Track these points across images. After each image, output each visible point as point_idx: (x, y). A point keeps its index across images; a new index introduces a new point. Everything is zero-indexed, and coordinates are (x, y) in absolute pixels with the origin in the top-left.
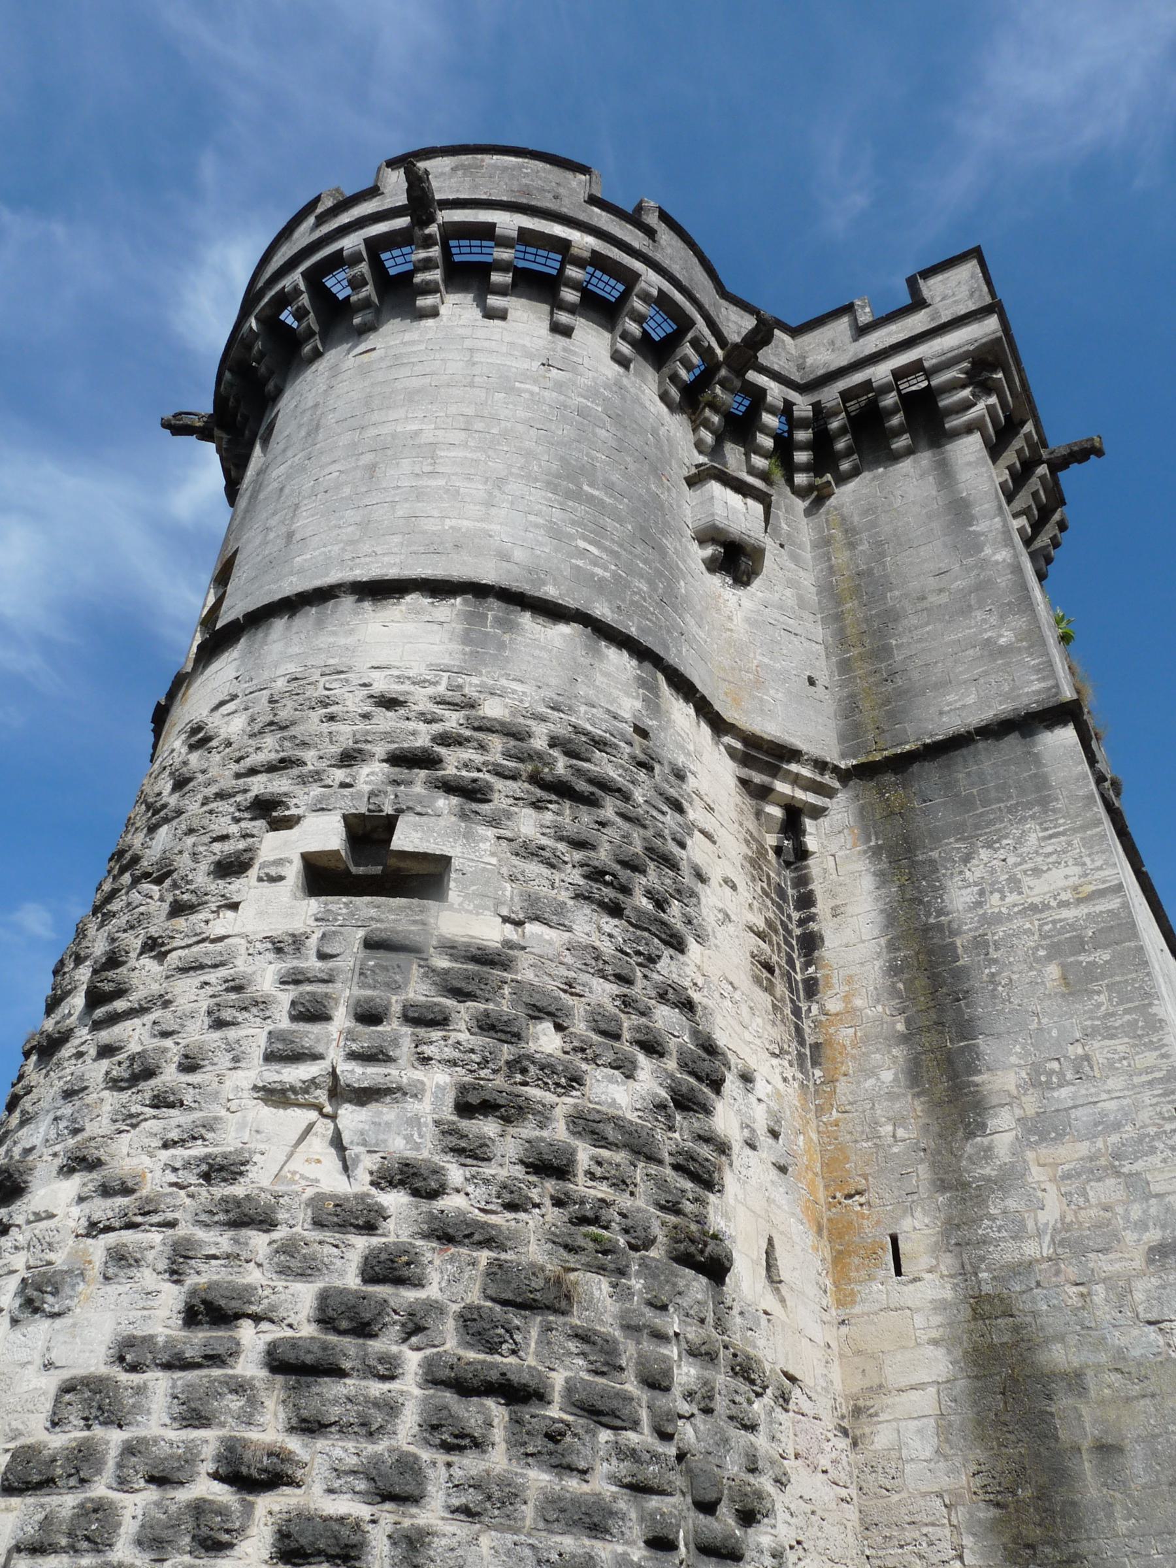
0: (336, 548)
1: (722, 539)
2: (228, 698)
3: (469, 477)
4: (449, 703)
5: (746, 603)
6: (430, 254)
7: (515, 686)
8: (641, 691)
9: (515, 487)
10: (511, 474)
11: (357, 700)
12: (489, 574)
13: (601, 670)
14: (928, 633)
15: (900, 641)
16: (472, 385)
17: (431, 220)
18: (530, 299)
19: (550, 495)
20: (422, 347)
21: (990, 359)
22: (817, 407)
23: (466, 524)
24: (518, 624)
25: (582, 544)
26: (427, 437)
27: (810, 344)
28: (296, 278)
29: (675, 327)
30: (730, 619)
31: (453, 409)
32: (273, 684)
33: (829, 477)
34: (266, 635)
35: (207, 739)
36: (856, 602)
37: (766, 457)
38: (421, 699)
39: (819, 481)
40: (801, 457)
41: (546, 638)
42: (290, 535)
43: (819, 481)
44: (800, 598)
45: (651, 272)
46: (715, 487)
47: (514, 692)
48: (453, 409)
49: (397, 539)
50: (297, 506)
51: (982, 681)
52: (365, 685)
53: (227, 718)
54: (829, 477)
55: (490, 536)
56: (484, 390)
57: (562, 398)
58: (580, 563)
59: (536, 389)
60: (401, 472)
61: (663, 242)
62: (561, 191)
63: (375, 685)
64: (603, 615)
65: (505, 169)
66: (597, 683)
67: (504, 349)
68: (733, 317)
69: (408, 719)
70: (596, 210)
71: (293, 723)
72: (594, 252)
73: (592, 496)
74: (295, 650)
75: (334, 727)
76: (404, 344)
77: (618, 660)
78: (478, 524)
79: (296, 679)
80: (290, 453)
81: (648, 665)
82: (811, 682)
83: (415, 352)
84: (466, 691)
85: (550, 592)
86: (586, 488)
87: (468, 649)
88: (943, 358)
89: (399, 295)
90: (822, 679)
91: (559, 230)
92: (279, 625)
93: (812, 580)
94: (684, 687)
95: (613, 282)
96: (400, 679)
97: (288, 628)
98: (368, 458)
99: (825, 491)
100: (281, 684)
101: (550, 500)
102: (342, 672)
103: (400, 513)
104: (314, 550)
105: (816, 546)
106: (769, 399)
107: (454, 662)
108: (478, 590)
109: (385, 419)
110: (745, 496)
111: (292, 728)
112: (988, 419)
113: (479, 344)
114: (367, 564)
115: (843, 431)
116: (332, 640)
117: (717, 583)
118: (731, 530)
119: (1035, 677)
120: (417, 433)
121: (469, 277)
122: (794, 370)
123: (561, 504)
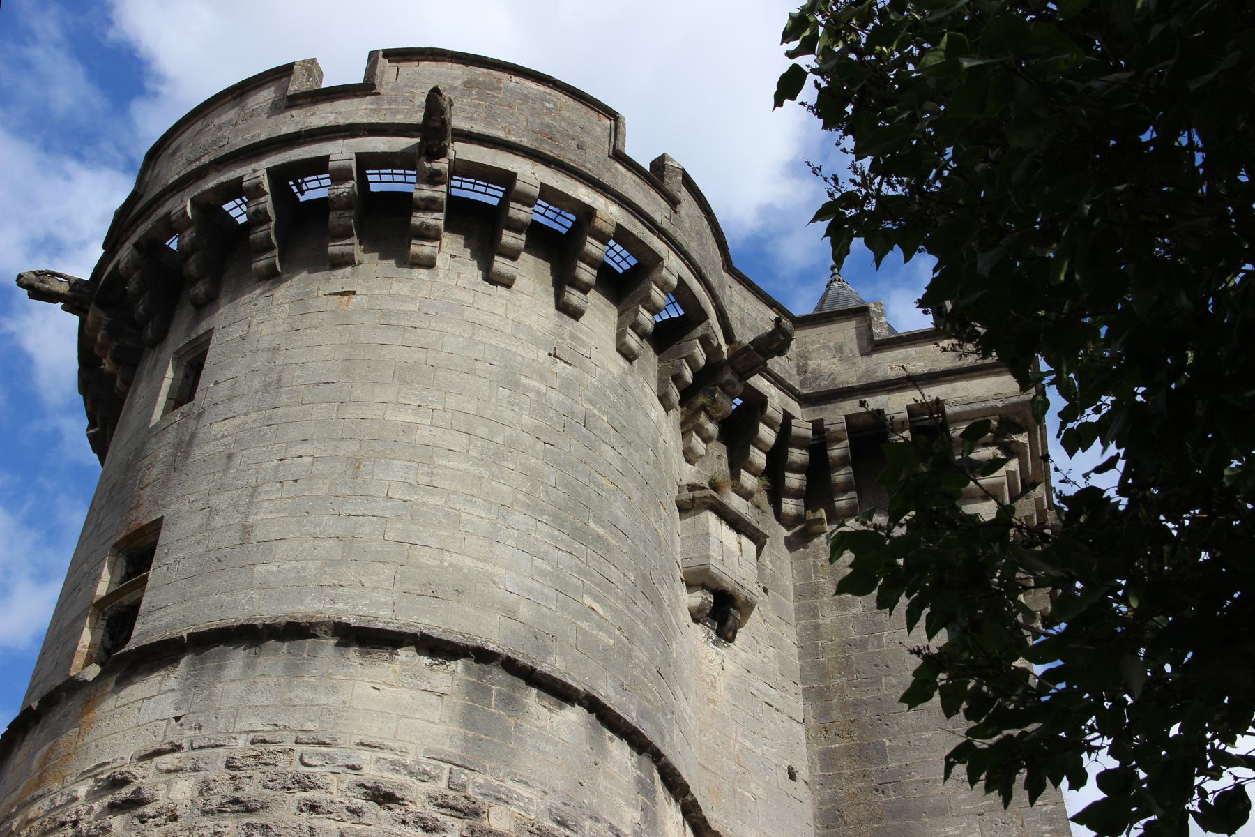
0: (312, 565)
1: (714, 587)
2: (167, 747)
3: (470, 499)
4: (452, 808)
5: (729, 665)
6: (436, 195)
7: (520, 789)
8: (641, 797)
9: (519, 518)
10: (516, 500)
11: (343, 787)
12: (494, 637)
13: (605, 772)
14: (928, 740)
15: (894, 743)
16: (473, 372)
17: (442, 153)
18: (537, 256)
19: (557, 533)
20: (414, 307)
21: (1018, 420)
22: (818, 426)
23: (468, 562)
24: (524, 706)
25: (588, 601)
26: (423, 434)
27: (813, 343)
28: (257, 172)
29: (682, 313)
30: (713, 686)
31: (452, 402)
32: (233, 742)
33: (822, 513)
34: (220, 667)
35: (136, 802)
36: (845, 679)
37: (755, 475)
38: (418, 795)
39: (811, 516)
40: (794, 480)
41: (552, 727)
42: (246, 531)
43: (811, 516)
44: (782, 660)
45: (673, 256)
46: (711, 518)
47: (520, 798)
48: (452, 402)
49: (388, 570)
50: (254, 491)
51: (986, 818)
52: (353, 768)
53: (166, 777)
54: (822, 513)
55: (495, 583)
56: (487, 382)
57: (569, 402)
58: (585, 625)
59: (543, 388)
60: (391, 476)
61: (683, 213)
62: (586, 138)
63: (366, 769)
64: (607, 697)
65: (526, 98)
66: (601, 788)
67: (508, 329)
68: (737, 299)
69: (404, 822)
70: (620, 168)
71: (265, 806)
72: (619, 226)
73: (599, 535)
74: (262, 699)
75: (317, 821)
76: (393, 296)
77: (619, 751)
78: (481, 565)
79: (264, 741)
80: (238, 406)
81: (646, 760)
82: (792, 776)
83: (405, 313)
84: (470, 791)
85: (553, 665)
86: (592, 525)
87: (470, 734)
88: (968, 408)
89: (387, 226)
90: (803, 774)
91: (583, 193)
92: (238, 658)
93: (795, 638)
94: (675, 785)
95: (625, 253)
96: (396, 767)
97: (250, 665)
98: (349, 448)
99: (815, 528)
100: (242, 741)
101: (555, 539)
102: (324, 744)
103: (391, 535)
104: (284, 561)
105: (799, 595)
106: (769, 409)
107: (450, 748)
108: (482, 656)
109: (369, 398)
110: (739, 532)
111: (262, 812)
112: (1006, 487)
113: (480, 317)
114: (352, 597)
115: (843, 462)
116: (308, 695)
117: (699, 636)
118: (725, 578)
119: (1047, 828)
120: (408, 429)
121: (481, 228)
122: (794, 372)
123: (567, 546)
